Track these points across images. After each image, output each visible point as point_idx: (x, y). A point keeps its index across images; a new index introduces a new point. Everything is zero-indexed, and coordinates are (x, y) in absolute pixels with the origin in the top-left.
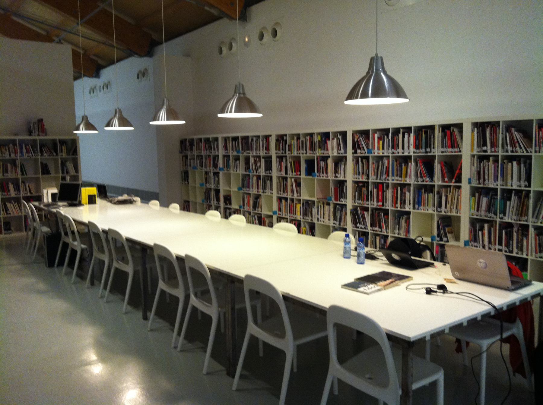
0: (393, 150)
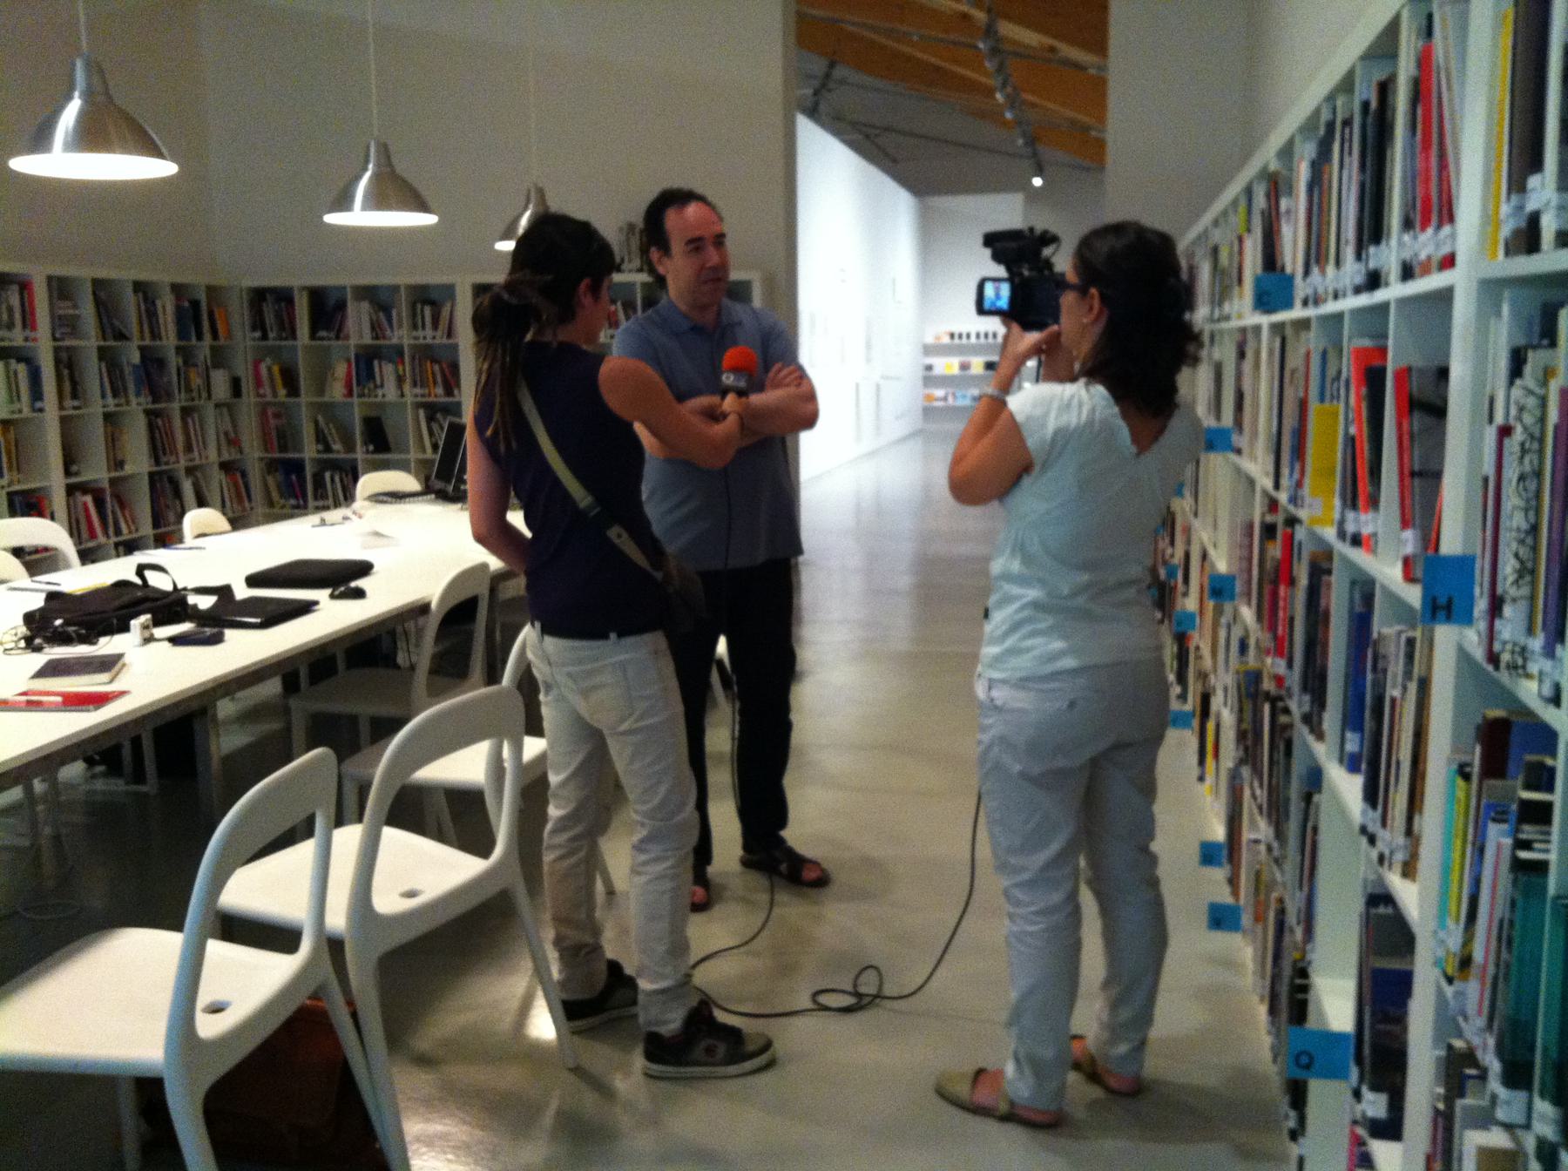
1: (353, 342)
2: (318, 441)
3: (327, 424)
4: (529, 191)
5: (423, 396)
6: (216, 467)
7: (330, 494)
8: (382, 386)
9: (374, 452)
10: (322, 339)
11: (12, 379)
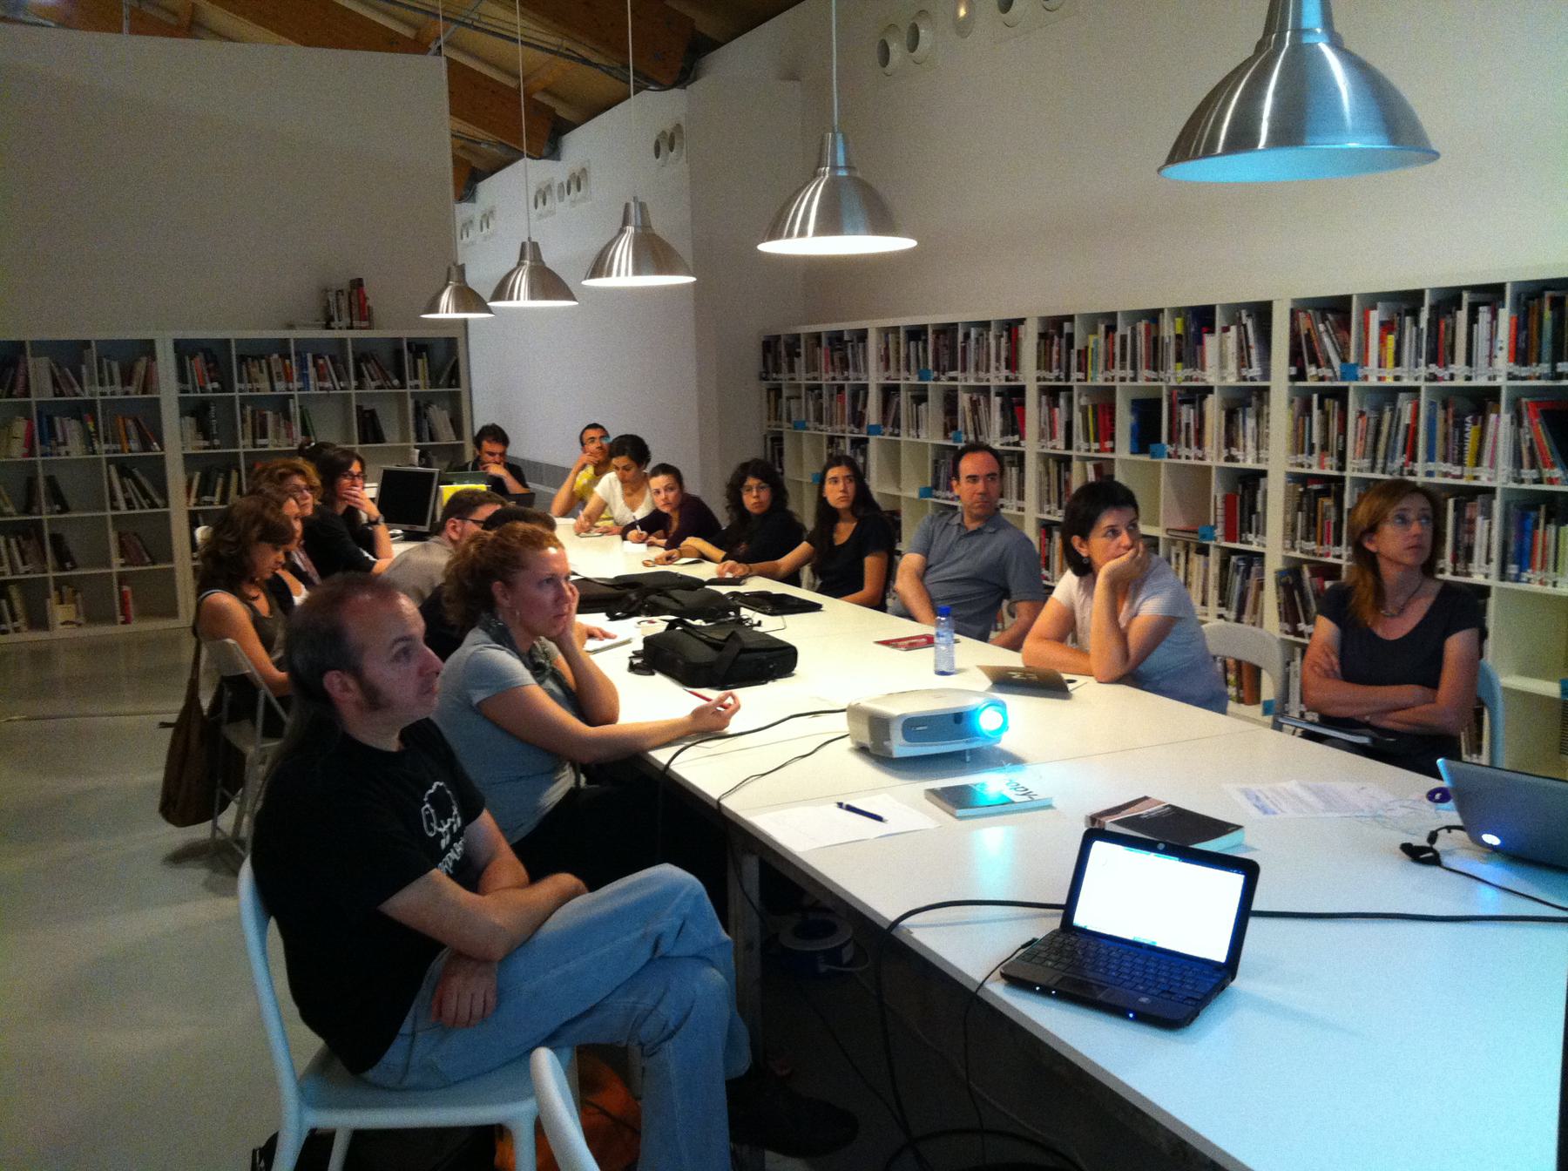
0: (1434, 368)
4: (627, 206)
5: (205, 448)
8: (65, 444)
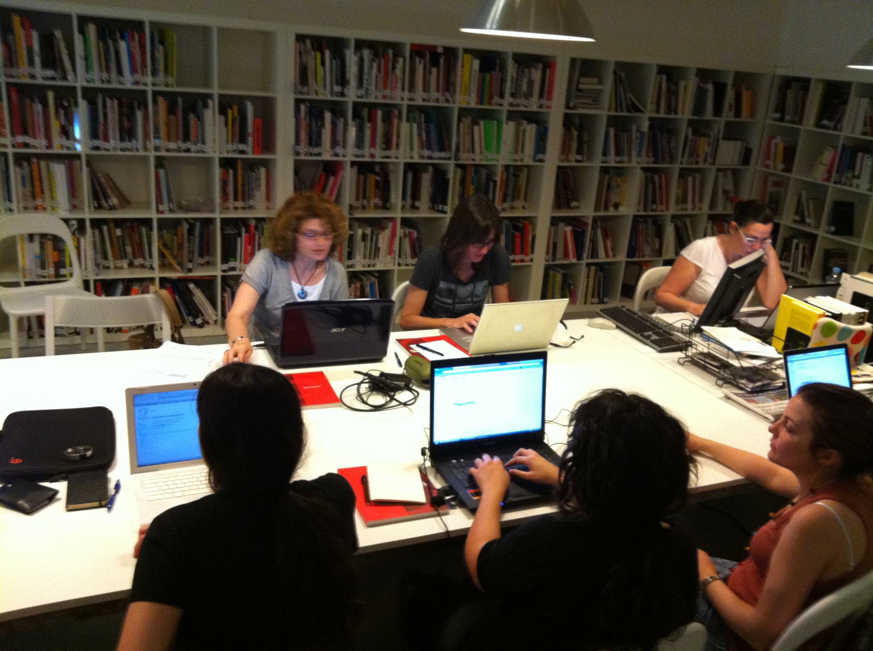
1: (842, 134)
2: (796, 213)
3: (808, 200)
6: (705, 218)
7: (792, 259)
9: (833, 233)
10: (824, 127)
11: (521, 135)
